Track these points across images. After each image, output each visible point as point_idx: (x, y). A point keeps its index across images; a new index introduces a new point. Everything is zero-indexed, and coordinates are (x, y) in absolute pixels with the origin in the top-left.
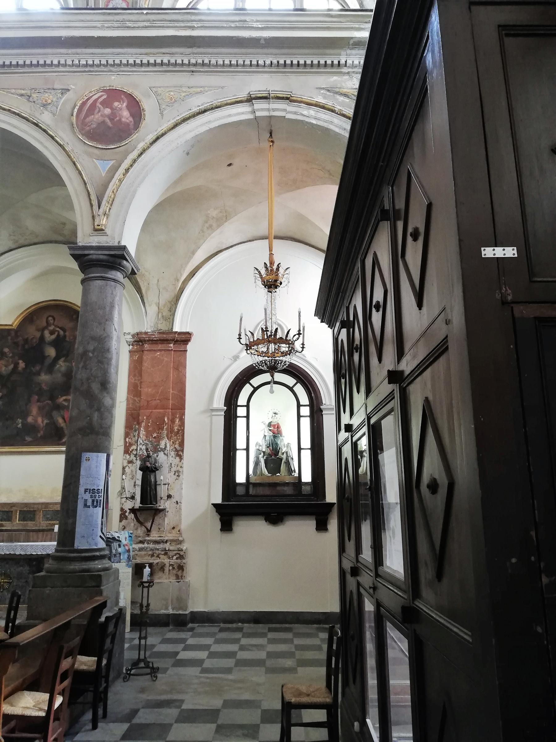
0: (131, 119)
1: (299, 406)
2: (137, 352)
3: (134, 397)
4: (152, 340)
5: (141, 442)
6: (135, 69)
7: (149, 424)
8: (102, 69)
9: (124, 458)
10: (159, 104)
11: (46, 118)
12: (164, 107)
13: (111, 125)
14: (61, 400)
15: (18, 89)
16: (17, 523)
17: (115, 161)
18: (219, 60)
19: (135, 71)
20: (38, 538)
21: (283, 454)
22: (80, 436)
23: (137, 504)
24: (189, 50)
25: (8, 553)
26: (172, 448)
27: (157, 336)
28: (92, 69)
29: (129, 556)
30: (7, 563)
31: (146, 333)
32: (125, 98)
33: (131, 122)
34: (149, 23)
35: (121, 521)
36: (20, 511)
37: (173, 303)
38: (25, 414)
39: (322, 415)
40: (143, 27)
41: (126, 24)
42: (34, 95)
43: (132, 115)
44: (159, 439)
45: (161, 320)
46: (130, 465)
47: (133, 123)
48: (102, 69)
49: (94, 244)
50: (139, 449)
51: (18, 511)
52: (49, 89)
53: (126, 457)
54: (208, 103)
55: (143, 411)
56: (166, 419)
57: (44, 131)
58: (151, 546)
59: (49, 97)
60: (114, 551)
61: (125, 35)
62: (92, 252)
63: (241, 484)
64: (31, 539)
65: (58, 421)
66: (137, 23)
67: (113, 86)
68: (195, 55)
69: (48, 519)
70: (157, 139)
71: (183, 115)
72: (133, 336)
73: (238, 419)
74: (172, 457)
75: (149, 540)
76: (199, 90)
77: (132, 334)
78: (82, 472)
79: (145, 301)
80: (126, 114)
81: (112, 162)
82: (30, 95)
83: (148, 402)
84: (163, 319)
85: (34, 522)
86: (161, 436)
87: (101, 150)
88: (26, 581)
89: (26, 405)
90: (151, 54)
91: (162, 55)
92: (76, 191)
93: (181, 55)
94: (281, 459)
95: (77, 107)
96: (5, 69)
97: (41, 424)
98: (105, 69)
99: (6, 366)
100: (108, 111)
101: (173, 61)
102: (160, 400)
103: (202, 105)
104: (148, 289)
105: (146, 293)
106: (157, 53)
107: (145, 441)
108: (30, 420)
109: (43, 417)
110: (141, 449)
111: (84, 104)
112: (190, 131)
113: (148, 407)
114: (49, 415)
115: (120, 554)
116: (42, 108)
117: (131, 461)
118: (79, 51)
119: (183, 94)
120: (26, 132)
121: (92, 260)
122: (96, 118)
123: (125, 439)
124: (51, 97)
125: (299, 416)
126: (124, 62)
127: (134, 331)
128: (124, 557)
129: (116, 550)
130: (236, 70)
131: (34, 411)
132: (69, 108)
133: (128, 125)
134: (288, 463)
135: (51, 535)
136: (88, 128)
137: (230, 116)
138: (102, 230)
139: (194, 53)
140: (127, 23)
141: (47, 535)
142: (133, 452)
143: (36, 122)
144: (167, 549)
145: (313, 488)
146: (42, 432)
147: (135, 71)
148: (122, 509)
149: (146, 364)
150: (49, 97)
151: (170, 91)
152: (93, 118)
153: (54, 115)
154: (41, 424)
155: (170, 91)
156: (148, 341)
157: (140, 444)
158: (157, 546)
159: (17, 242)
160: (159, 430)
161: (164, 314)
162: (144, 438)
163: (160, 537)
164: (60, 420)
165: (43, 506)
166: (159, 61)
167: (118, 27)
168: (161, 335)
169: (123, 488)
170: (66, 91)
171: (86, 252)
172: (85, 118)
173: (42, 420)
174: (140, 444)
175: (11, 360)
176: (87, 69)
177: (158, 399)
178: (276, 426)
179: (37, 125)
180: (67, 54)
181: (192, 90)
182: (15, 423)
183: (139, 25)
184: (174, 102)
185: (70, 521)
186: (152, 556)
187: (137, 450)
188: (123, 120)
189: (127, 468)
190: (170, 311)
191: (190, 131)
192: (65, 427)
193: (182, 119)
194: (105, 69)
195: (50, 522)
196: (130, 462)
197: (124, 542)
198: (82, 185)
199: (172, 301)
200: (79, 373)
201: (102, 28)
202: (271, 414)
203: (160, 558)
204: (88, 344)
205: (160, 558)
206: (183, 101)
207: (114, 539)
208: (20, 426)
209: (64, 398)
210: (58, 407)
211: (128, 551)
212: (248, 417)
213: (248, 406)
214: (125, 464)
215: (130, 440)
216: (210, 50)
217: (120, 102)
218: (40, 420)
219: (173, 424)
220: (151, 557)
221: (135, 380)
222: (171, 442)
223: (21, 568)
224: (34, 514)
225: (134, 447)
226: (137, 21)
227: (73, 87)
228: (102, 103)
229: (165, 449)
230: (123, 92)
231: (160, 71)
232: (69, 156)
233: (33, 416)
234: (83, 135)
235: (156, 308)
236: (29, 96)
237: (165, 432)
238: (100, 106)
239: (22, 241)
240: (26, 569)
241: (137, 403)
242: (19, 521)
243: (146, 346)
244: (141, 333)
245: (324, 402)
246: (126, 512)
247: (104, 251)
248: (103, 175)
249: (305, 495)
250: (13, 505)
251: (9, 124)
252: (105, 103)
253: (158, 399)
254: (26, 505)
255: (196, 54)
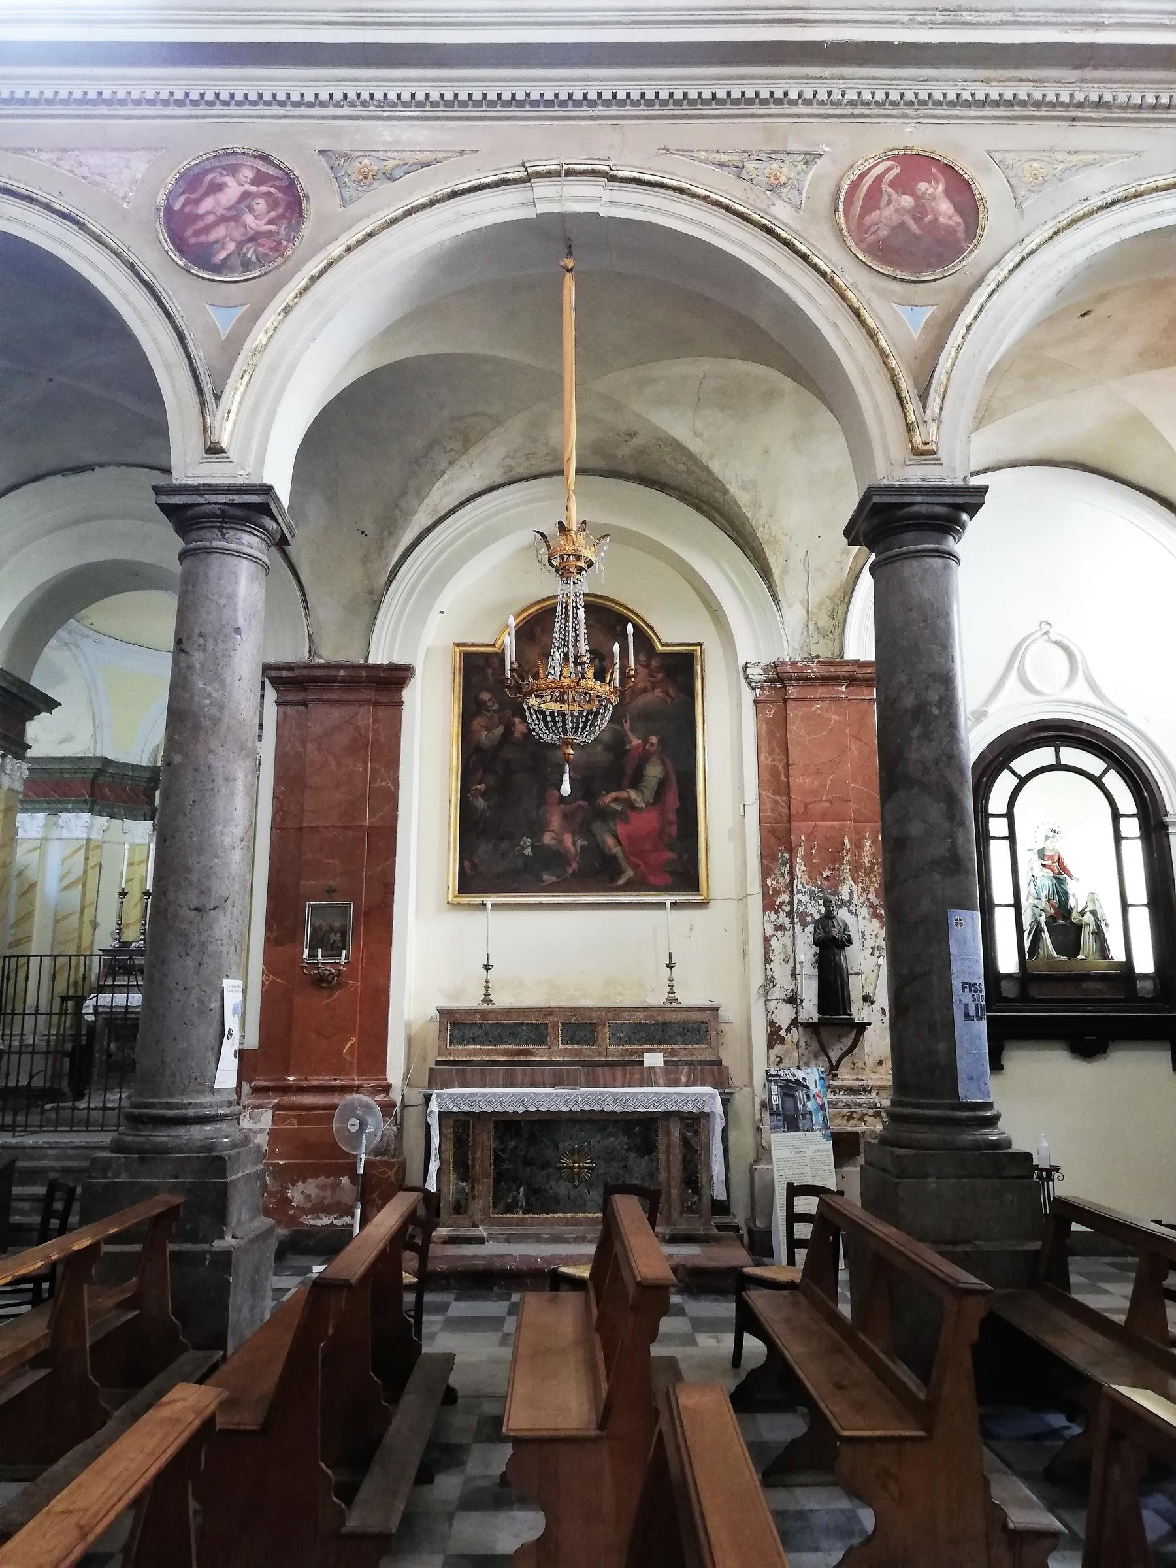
0: (957, 219)
1: (1116, 816)
2: (772, 702)
3: (773, 794)
4: (807, 679)
5: (800, 886)
6: (955, 112)
7: (813, 851)
8: (888, 112)
9: (766, 918)
10: (1011, 185)
11: (781, 213)
12: (1022, 193)
13: (918, 232)
14: (607, 799)
15: (712, 151)
16: (558, 1050)
17: (935, 307)
18: (1134, 95)
19: (958, 117)
20: (614, 1076)
21: (1082, 914)
22: (938, 878)
23: (810, 1010)
24: (1076, 74)
25: (587, 1108)
26: (862, 900)
27: (815, 670)
28: (867, 112)
29: (825, 1116)
30: (581, 1130)
31: (794, 664)
32: (940, 176)
33: (958, 224)
34: (1009, 14)
35: (770, 1046)
36: (563, 1024)
37: (837, 601)
38: (537, 828)
39: (1167, 835)
40: (995, 24)
41: (962, 15)
42: (750, 166)
43: (958, 210)
44: (835, 882)
45: (815, 635)
46: (779, 933)
47: (962, 227)
48: (888, 110)
49: (913, 483)
50: (796, 901)
51: (560, 1025)
52: (776, 152)
53: (769, 917)
54: (1121, 186)
55: (797, 824)
56: (846, 842)
57: (786, 243)
58: (844, 1098)
59: (785, 171)
60: (801, 1107)
61: (956, 41)
62: (919, 499)
63: (1009, 976)
64: (602, 1081)
65: (604, 842)
66: (985, 14)
67: (912, 149)
68: (1086, 85)
69: (620, 1041)
70: (1023, 260)
71: (1071, 212)
72: (765, 670)
73: (992, 842)
74: (864, 918)
75: (836, 1087)
76: (1090, 158)
77: (762, 665)
78: (953, 949)
79: (781, 596)
80: (945, 207)
81: (930, 311)
82: (740, 165)
83: (806, 805)
84: (819, 633)
85: (595, 1047)
86: (839, 876)
87: (904, 285)
88: (625, 1166)
89: (539, 807)
90: (994, 80)
91: (1016, 84)
92: (862, 371)
93: (1055, 84)
94: (1078, 928)
95: (843, 193)
96: (511, 109)
97: (572, 849)
98: (895, 112)
99: (489, 729)
100: (907, 201)
101: (1038, 95)
102: (831, 802)
103: (1110, 190)
104: (785, 571)
105: (783, 583)
106: (1008, 80)
107: (808, 884)
108: (548, 839)
109: (573, 835)
110: (800, 901)
111: (855, 185)
112: (1083, 246)
113: (806, 816)
114: (584, 830)
115: (810, 1113)
116: (768, 193)
117: (781, 926)
118: (847, 71)
119: (1060, 167)
120: (742, 245)
121: (917, 516)
122: (885, 215)
123: (763, 880)
124: (784, 169)
125: (1118, 838)
126: (750, 94)
127: (767, 660)
128: (817, 1119)
129: (804, 1105)
130: (1165, 116)
131: (556, 821)
132: (825, 193)
133: (952, 231)
134: (1099, 934)
135: (642, 1073)
136: (872, 237)
137: (1161, 213)
138: (934, 453)
139: (1082, 81)
140: (964, 14)
141: (632, 1074)
142: (783, 907)
143: (767, 223)
144: (879, 1105)
145: (1159, 987)
146: (575, 865)
147: (958, 117)
148: (771, 1023)
149: (795, 729)
150: (785, 171)
151: (1030, 160)
152: (880, 216)
153: (798, 208)
154: (572, 849)
155: (1030, 160)
156: (797, 679)
157: (799, 890)
158: (858, 1099)
159: (511, 468)
160: (834, 863)
161: (820, 624)
162: (805, 878)
163: (858, 1079)
164: (610, 841)
165: (610, 1015)
166: (1023, 96)
167: (944, 23)
168: (824, 668)
169: (770, 980)
170: (813, 157)
171: (907, 499)
172: (862, 217)
173: (574, 840)
174: (799, 890)
175: (496, 717)
176: (856, 112)
177: (826, 801)
178: (1056, 859)
179: (769, 231)
180: (820, 78)
181: (1075, 158)
182: (519, 845)
183: (987, 19)
184: (1042, 184)
185: (942, 1046)
186: (850, 1117)
187: (791, 903)
188: (942, 220)
189: (774, 940)
190: (832, 616)
191: (1083, 246)
192: (620, 855)
193: (1070, 219)
194: (895, 112)
195: (626, 1047)
196: (779, 927)
197: (814, 1090)
198: (877, 360)
199: (835, 596)
200: (913, 747)
201: (912, 24)
202: (1045, 831)
203: (865, 1122)
204: (927, 688)
205: (865, 1122)
206: (1061, 180)
207: (797, 1082)
208: (528, 851)
209: (614, 795)
210: (604, 815)
211: (822, 1108)
212: (1011, 838)
213: (1010, 815)
214: (769, 930)
215: (774, 883)
216: (1118, 74)
217: (930, 182)
218: (568, 839)
219: (859, 852)
220: (848, 1120)
221: (773, 760)
222: (860, 889)
223: (612, 1139)
224: (593, 1031)
225: (785, 897)
226: (986, 11)
227: (827, 149)
228: (892, 184)
229: (850, 901)
230: (922, 159)
231: (1008, 118)
232: (843, 297)
233: (553, 831)
234: (864, 251)
235: (803, 613)
236: (741, 168)
237: (847, 867)
238: (890, 190)
239: (520, 471)
240: (618, 1141)
241: (783, 807)
242: (562, 1044)
243: (791, 689)
244: (784, 663)
245: (1169, 808)
246: (780, 1028)
247: (883, 497)
248: (916, 338)
249: (1143, 999)
250: (548, 1012)
251: (706, 227)
252: (902, 185)
253: (826, 801)
254: (576, 1011)
255: (1088, 81)
